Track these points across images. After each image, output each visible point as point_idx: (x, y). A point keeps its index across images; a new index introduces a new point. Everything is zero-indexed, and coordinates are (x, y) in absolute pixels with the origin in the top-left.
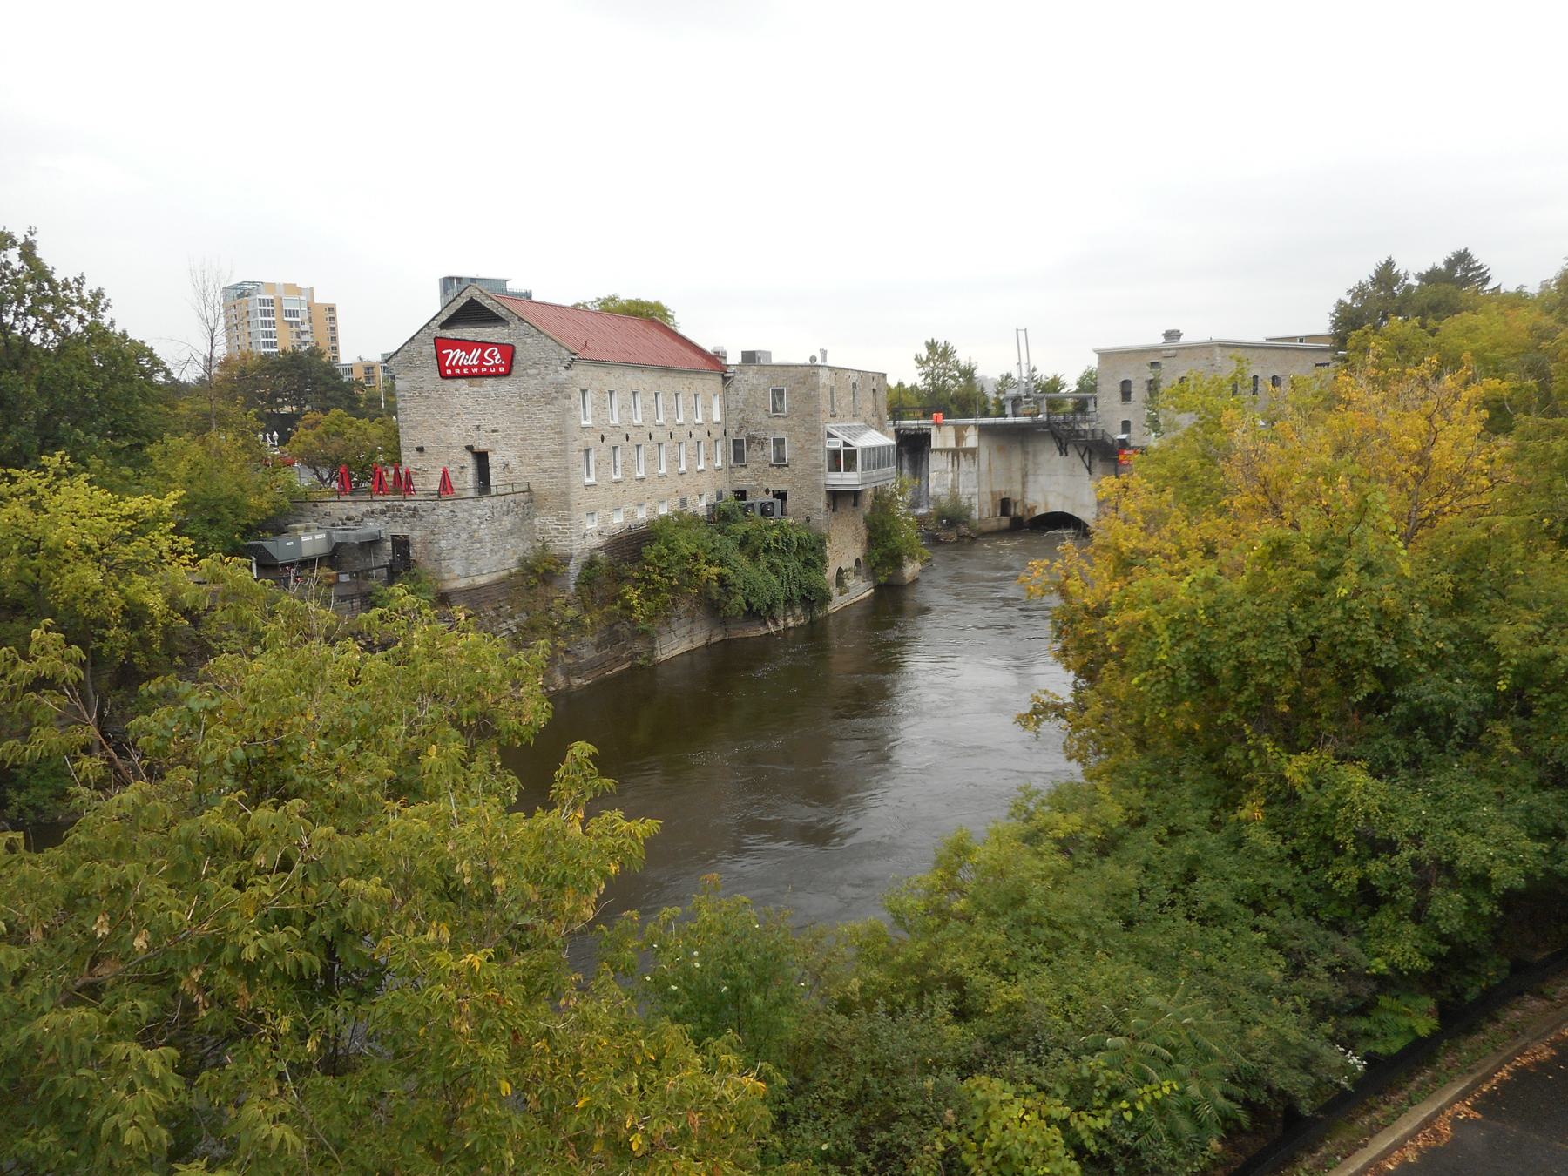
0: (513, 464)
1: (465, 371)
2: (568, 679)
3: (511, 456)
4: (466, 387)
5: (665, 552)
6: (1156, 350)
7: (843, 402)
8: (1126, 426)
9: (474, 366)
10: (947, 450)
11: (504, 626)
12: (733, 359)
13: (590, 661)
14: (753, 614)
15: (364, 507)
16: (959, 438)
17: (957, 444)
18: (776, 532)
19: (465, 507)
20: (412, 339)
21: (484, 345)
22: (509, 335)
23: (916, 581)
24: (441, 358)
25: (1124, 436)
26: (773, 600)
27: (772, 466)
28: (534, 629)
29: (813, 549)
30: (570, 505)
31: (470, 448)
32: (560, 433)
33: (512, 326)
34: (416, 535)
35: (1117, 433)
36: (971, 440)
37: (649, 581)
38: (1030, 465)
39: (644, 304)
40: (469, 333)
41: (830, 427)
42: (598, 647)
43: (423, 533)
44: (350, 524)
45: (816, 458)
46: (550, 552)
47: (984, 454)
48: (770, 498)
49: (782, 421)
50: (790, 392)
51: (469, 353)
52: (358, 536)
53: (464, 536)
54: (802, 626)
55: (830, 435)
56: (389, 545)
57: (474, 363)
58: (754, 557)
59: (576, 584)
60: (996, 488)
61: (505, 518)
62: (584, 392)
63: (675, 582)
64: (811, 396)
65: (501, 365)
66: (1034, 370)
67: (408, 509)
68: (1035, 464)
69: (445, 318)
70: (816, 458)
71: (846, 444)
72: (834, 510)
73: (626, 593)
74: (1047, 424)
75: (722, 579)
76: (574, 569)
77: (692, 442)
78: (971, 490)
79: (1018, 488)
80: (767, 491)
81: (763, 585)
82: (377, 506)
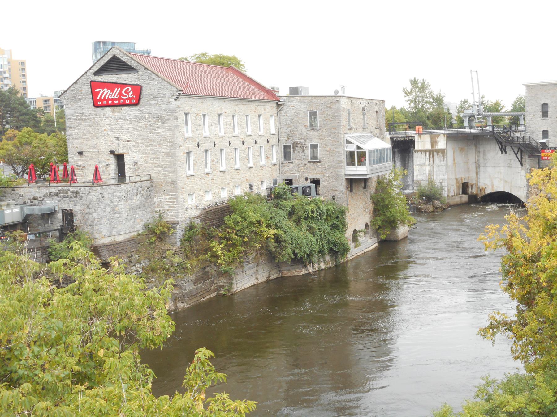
1: (110, 102)
2: (175, 303)
4: (110, 113)
5: (239, 219)
7: (356, 120)
9: (115, 99)
10: (426, 151)
11: (134, 268)
12: (284, 92)
13: (190, 291)
14: (297, 261)
15: (45, 191)
16: (433, 143)
17: (432, 146)
18: (312, 206)
19: (109, 190)
20: (76, 82)
21: (122, 85)
23: (405, 238)
24: (94, 94)
26: (311, 251)
27: (309, 162)
28: (153, 270)
29: (337, 217)
30: (177, 189)
31: (112, 152)
32: (171, 142)
33: (140, 73)
34: (77, 209)
35: (539, 139)
36: (442, 143)
37: (228, 239)
38: (481, 160)
39: (224, 58)
40: (112, 78)
41: (347, 137)
42: (195, 282)
43: (82, 208)
44: (36, 202)
45: (339, 157)
46: (164, 220)
47: (450, 154)
48: (308, 183)
49: (316, 133)
50: (322, 114)
51: (112, 91)
52: (41, 210)
53: (109, 209)
54: (330, 268)
55: (348, 142)
56: (60, 216)
57: (116, 97)
58: (298, 222)
59: (181, 241)
60: (459, 176)
61: (135, 197)
62: (186, 115)
63: (246, 239)
64: (335, 117)
65: (133, 98)
66: (483, 97)
67: (73, 192)
68: (484, 159)
70: (339, 157)
71: (358, 148)
72: (351, 191)
73: (214, 247)
74: (493, 133)
75: (277, 238)
76: (179, 232)
77: (257, 146)
78: (442, 177)
79: (473, 175)
80: (306, 179)
81: (304, 241)
82: (53, 190)
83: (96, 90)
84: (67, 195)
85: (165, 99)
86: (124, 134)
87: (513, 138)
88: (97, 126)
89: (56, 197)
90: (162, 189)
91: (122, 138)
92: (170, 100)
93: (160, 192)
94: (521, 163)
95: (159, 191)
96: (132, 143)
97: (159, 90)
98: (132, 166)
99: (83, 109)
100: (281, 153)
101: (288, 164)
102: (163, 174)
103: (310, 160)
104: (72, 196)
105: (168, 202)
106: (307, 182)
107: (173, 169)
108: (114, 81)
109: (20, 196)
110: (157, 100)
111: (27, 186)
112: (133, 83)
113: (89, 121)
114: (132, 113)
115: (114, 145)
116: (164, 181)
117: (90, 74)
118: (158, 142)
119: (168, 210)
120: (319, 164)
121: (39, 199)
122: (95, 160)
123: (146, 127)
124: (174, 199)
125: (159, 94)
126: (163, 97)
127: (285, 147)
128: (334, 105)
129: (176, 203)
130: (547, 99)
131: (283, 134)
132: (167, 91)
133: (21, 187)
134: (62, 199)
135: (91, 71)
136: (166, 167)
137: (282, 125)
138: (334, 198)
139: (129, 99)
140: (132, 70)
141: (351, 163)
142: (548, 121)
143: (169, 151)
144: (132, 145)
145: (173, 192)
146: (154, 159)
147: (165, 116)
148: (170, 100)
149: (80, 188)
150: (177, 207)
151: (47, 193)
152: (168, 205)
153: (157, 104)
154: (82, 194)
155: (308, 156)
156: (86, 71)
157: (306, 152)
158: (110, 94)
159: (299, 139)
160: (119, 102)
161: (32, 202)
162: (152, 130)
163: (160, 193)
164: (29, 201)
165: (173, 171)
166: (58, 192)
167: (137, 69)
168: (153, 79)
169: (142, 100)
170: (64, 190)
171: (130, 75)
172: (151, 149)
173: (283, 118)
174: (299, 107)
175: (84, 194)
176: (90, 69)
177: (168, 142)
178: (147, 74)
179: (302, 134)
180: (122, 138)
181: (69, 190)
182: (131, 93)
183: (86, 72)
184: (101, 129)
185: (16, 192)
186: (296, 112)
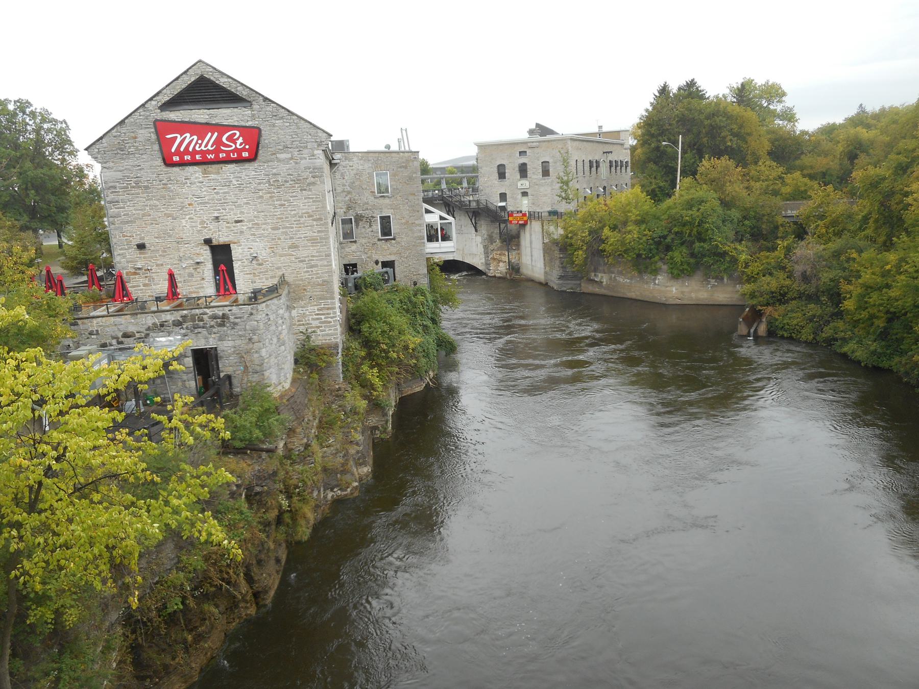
0: (263, 254)
1: (198, 157)
3: (260, 248)
6: (524, 143)
8: (503, 197)
9: (209, 152)
20: (122, 123)
21: (221, 129)
22: (253, 117)
24: (164, 145)
25: (503, 204)
27: (379, 240)
31: (208, 242)
32: (320, 219)
33: (256, 106)
35: (496, 201)
40: (200, 115)
45: (420, 231)
49: (387, 201)
51: (202, 137)
53: (275, 340)
57: (209, 147)
65: (244, 150)
67: (214, 317)
69: (167, 99)
70: (420, 231)
80: (377, 263)
83: (168, 137)
84: (201, 323)
85: (306, 151)
86: (230, 209)
87: (464, 202)
88: (172, 199)
89: (177, 329)
90: (306, 295)
91: (226, 217)
92: (316, 152)
93: (302, 300)
94: (475, 228)
95: (300, 298)
96: (246, 225)
97: (294, 136)
98: (246, 263)
99: (140, 169)
100: (339, 230)
101: (350, 244)
102: (308, 272)
103: (380, 237)
104: (212, 323)
105: (318, 314)
106: (378, 266)
107: (326, 263)
108: (203, 121)
109: (91, 333)
110: (291, 152)
111: (105, 313)
112: (243, 124)
113: (154, 191)
114: (243, 175)
116: (309, 283)
117: (151, 108)
118: (295, 221)
119: (318, 327)
120: (393, 241)
121: (138, 335)
122: (172, 256)
123: (271, 197)
124: (328, 309)
125: (294, 143)
126: (301, 147)
127: (344, 222)
128: (411, 164)
129: (332, 315)
130: (503, 159)
131: (340, 205)
133: (93, 317)
134: (192, 331)
135: (153, 103)
136: (313, 260)
137: (337, 191)
138: (415, 284)
139: (236, 150)
140: (240, 102)
141: (432, 238)
142: (506, 183)
143: (316, 234)
145: (327, 299)
146: (289, 248)
147: (307, 179)
148: (316, 152)
149: (230, 308)
150: (334, 321)
151: (154, 324)
152: (318, 319)
153: (292, 158)
154: (236, 318)
155: (378, 232)
156: (143, 102)
157: (374, 227)
158: (197, 143)
159: (363, 210)
160: (217, 156)
161: (119, 343)
162: (283, 202)
163: (302, 303)
164: (114, 342)
165: (325, 266)
166: (180, 319)
167: (249, 100)
168: (282, 118)
169: (260, 152)
171: (236, 110)
172: (283, 233)
173: (338, 183)
174: (361, 167)
175: (240, 318)
176: (151, 99)
177: (314, 220)
179: (367, 203)
180: (226, 217)
181: (205, 314)
182: (241, 140)
183: (143, 105)
184: (182, 203)
185: (81, 327)
186: (357, 174)
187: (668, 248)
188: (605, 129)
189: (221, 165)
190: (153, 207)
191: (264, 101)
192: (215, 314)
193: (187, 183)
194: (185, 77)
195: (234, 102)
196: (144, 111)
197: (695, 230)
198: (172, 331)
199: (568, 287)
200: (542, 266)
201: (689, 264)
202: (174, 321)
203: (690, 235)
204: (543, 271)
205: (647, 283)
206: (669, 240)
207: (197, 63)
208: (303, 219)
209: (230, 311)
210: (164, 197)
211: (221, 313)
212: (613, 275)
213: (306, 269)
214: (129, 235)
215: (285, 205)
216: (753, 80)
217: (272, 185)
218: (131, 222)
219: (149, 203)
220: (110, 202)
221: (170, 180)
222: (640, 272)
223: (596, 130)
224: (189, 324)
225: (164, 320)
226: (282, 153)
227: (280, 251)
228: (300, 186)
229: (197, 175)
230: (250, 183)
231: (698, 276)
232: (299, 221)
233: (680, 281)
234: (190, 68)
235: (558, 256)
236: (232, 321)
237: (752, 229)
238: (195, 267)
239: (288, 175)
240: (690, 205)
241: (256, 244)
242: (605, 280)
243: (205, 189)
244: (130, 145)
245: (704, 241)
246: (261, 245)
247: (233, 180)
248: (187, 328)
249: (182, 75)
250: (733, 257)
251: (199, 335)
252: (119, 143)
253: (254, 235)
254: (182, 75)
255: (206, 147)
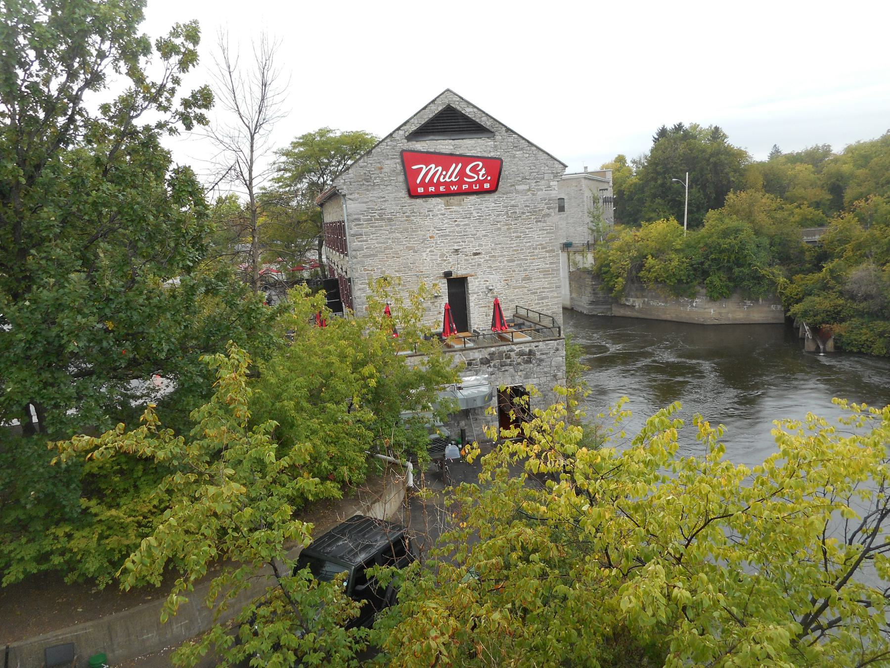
1: (442, 189)
3: (496, 281)
9: (452, 183)
21: (466, 160)
24: (409, 175)
33: (498, 137)
40: (444, 145)
51: (446, 168)
57: (453, 179)
65: (486, 181)
67: (521, 354)
69: (414, 128)
83: (414, 167)
84: (508, 361)
85: (543, 182)
86: (469, 242)
88: (414, 231)
89: (484, 367)
91: (465, 250)
92: (552, 183)
97: (532, 167)
99: (385, 201)
104: (519, 360)
107: (556, 295)
108: (448, 152)
110: (529, 184)
112: (486, 155)
114: (483, 207)
115: (449, 263)
118: (529, 253)
125: (532, 174)
132: (544, 169)
135: (401, 132)
136: (543, 292)
139: (478, 181)
140: (482, 133)
143: (548, 266)
144: (482, 260)
146: (523, 280)
147: (543, 210)
148: (552, 183)
149: (537, 344)
153: (529, 190)
158: (441, 174)
160: (460, 187)
166: (488, 357)
167: (493, 130)
168: (522, 149)
169: (500, 183)
170: (501, 353)
171: (479, 140)
172: (517, 265)
176: (399, 129)
177: (547, 252)
178: (510, 140)
180: (465, 250)
181: (512, 350)
182: (483, 171)
183: (391, 135)
184: (424, 235)
187: (705, 273)
188: (589, 170)
189: (463, 197)
190: (396, 240)
191: (506, 132)
192: (522, 350)
193: (429, 215)
194: (433, 107)
195: (478, 133)
196: (391, 141)
197: (733, 256)
198: (480, 370)
199: (599, 311)
200: (568, 292)
201: (727, 287)
202: (482, 359)
203: (728, 261)
204: (568, 297)
205: (683, 306)
206: (706, 266)
207: (445, 92)
208: (537, 251)
209: (536, 347)
210: (406, 230)
211: (527, 350)
212: (646, 300)
213: (536, 302)
214: (370, 269)
215: (521, 237)
216: (698, 125)
217: (510, 217)
218: (373, 255)
219: (391, 236)
220: (354, 235)
221: (413, 212)
222: (677, 297)
223: (583, 171)
224: (496, 362)
225: (472, 358)
226: (521, 184)
227: (513, 283)
228: (536, 218)
229: (439, 207)
230: (490, 215)
231: (735, 297)
232: (533, 252)
233: (718, 303)
234: (438, 97)
235: (590, 283)
236: (538, 357)
237: (779, 254)
238: (432, 301)
239: (526, 206)
240: (725, 234)
241: (492, 276)
242: (637, 304)
243: (446, 221)
244: (376, 175)
245: (742, 266)
246: (497, 277)
247: (474, 212)
248: (494, 366)
249: (430, 104)
250: (770, 280)
251: (506, 373)
252: (365, 173)
253: (490, 267)
254: (430, 104)
255: (449, 178)
